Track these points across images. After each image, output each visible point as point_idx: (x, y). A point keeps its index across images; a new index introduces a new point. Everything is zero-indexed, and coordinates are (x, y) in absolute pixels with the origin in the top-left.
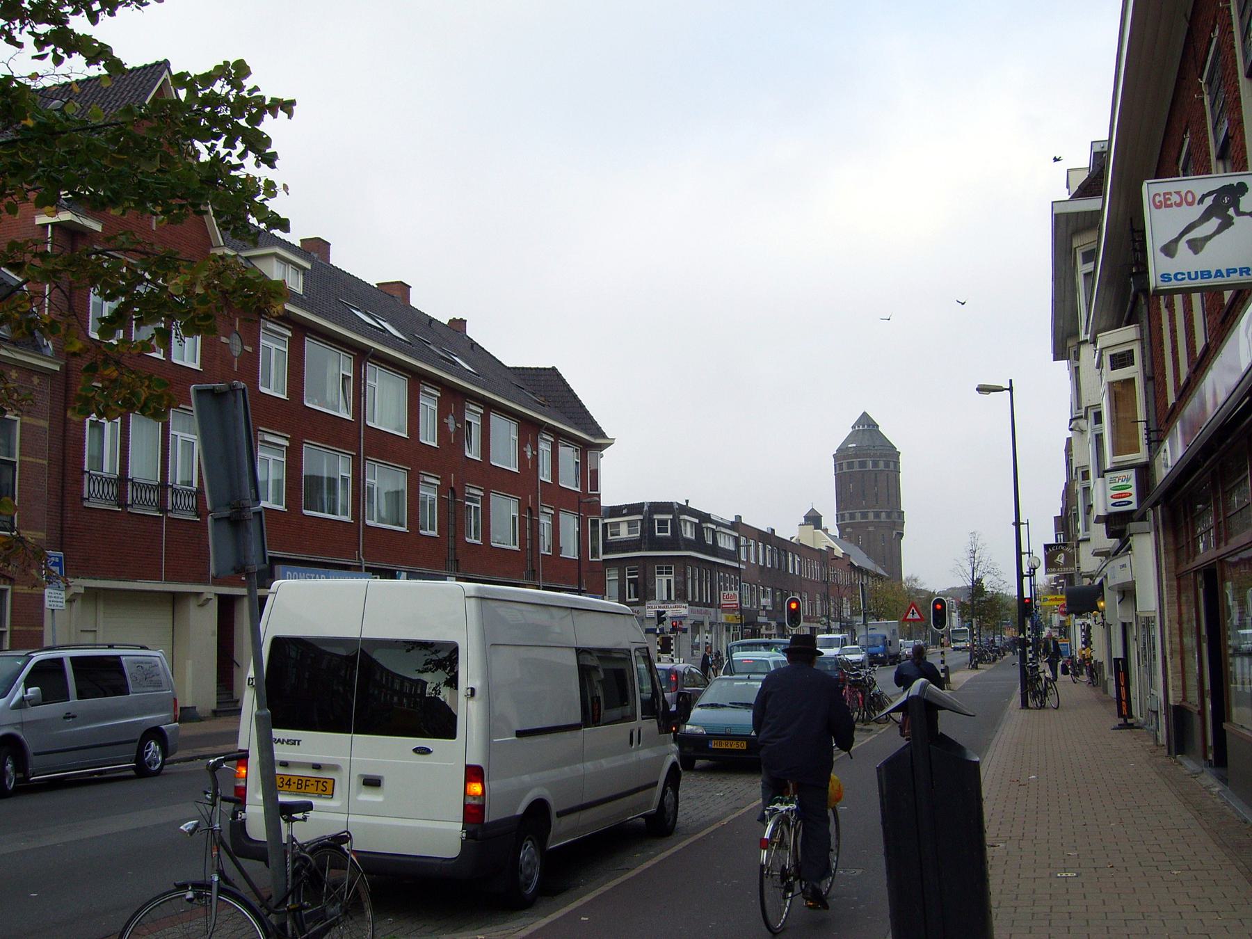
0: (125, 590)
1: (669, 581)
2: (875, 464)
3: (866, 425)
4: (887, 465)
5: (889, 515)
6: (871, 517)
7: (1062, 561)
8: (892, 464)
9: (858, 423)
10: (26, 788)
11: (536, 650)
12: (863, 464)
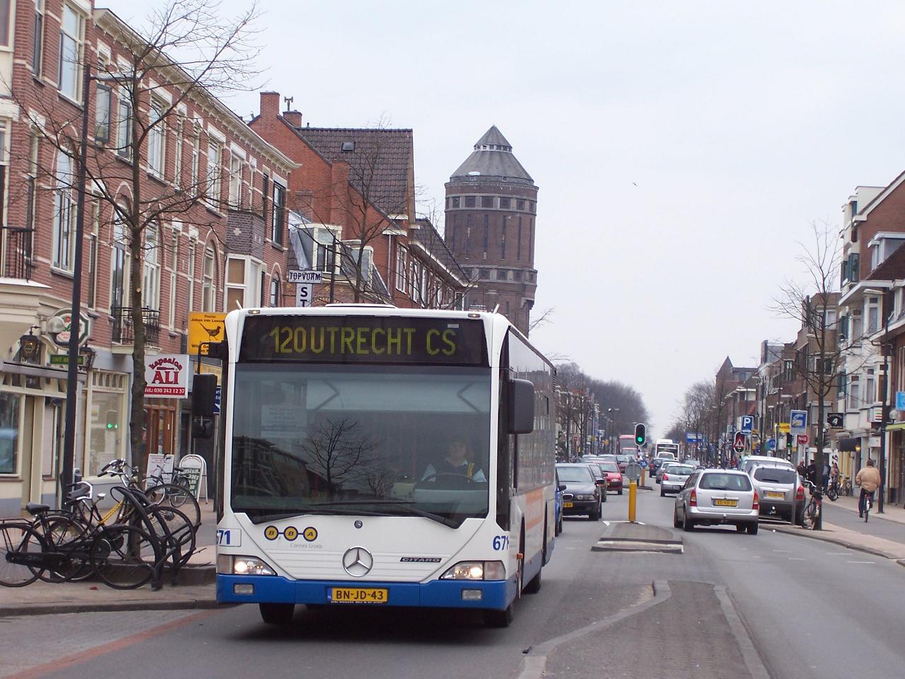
0: (289, 317)
1: (206, 309)
2: (505, 202)
3: (495, 145)
4: (521, 204)
5: (518, 275)
6: (493, 275)
7: (836, 423)
8: (527, 204)
9: (485, 141)
10: (483, 562)
11: (856, 543)
12: (488, 201)
